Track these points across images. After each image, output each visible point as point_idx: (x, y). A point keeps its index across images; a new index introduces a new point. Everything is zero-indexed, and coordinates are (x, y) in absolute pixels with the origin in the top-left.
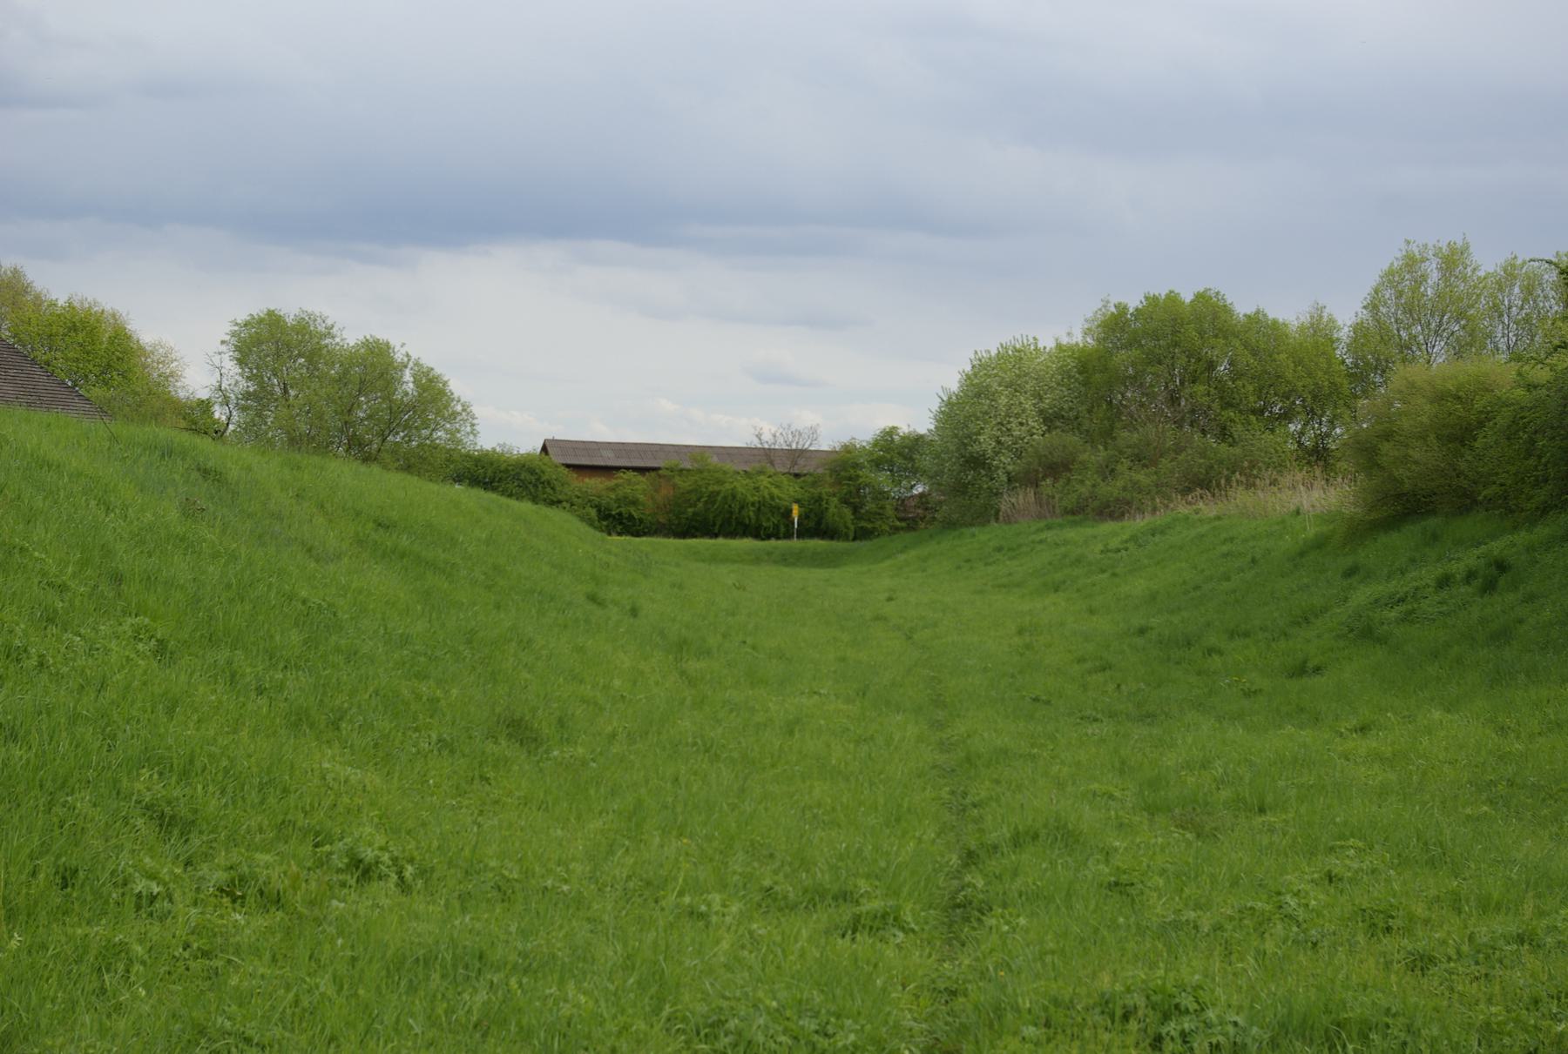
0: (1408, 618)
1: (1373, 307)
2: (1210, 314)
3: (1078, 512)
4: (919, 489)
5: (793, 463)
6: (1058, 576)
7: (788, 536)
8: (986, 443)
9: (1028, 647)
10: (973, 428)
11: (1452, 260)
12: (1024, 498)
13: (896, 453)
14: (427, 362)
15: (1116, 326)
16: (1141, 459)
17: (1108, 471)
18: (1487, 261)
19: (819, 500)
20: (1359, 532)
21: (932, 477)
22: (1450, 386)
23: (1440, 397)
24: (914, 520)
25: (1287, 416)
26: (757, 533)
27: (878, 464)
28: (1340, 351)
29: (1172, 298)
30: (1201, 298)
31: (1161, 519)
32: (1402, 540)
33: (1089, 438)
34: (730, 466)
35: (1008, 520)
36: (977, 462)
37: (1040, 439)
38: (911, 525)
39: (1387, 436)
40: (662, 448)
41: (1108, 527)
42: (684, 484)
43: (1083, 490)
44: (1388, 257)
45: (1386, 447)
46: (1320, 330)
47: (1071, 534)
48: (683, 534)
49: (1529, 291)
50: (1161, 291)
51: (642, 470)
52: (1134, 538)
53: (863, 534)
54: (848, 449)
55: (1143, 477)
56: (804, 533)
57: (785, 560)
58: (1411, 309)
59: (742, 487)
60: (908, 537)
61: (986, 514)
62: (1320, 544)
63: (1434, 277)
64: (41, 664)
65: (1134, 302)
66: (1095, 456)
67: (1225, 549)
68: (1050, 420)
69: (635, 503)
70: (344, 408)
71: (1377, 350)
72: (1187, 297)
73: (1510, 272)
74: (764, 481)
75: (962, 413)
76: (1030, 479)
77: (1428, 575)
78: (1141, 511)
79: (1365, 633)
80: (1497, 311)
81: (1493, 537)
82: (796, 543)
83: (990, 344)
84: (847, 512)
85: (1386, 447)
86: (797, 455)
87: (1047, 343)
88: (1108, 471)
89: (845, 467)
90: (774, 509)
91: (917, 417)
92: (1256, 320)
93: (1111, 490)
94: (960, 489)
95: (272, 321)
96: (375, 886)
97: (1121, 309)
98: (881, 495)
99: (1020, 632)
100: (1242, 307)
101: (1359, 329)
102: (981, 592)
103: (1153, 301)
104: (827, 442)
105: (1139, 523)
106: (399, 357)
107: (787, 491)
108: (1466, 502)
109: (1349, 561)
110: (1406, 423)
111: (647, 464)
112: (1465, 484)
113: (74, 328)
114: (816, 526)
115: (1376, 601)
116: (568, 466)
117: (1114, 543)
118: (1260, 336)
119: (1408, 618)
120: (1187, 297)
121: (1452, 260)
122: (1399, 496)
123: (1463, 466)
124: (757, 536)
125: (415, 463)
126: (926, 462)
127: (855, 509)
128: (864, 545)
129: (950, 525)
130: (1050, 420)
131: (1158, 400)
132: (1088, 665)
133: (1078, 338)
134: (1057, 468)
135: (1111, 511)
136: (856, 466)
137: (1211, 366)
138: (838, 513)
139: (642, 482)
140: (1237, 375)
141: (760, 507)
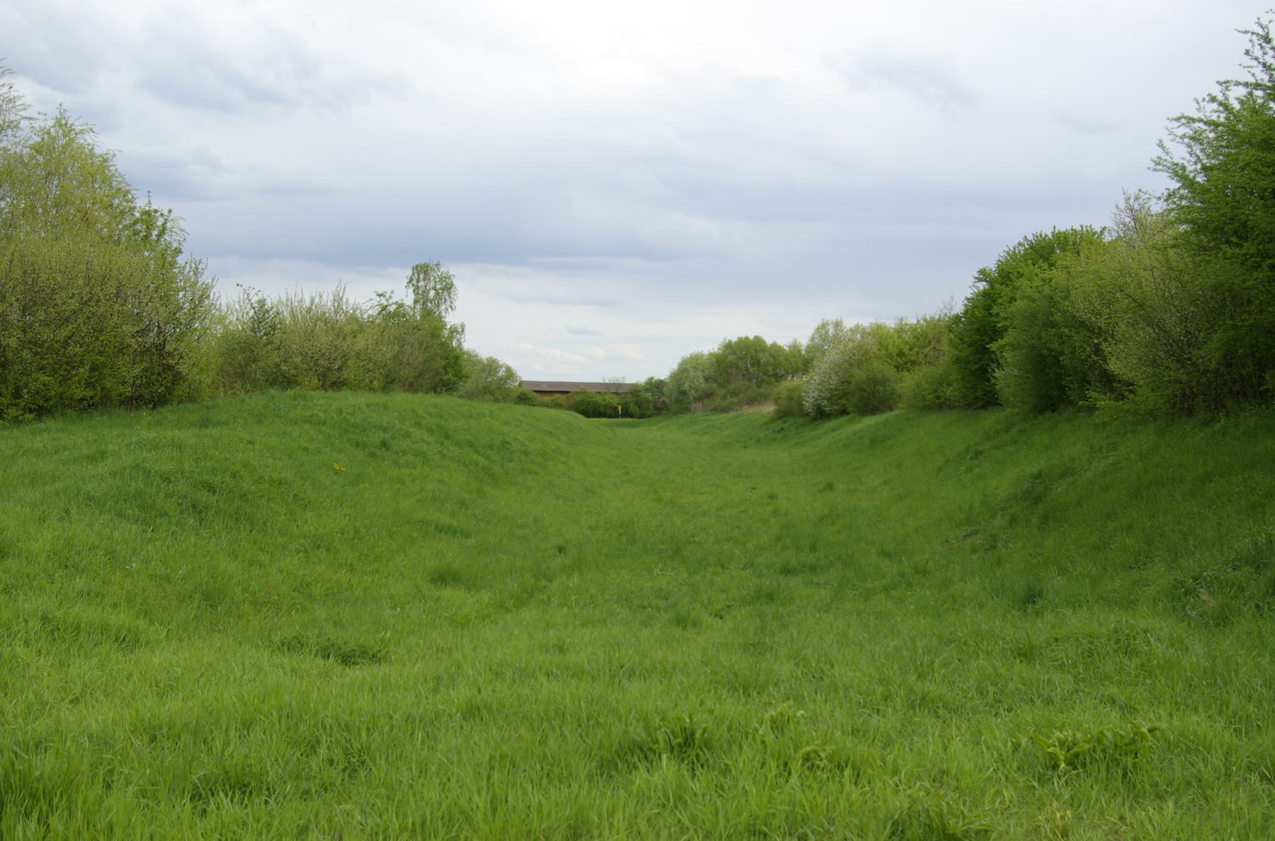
1: (812, 339)
2: (758, 342)
5: (616, 389)
7: (617, 416)
8: (686, 387)
11: (837, 325)
12: (699, 405)
13: (655, 386)
15: (729, 346)
16: (734, 394)
17: (724, 397)
20: (773, 420)
26: (610, 416)
27: (647, 390)
29: (747, 338)
33: (720, 385)
36: (684, 393)
41: (723, 415)
44: (817, 323)
46: (795, 347)
47: (712, 417)
50: (743, 336)
53: (642, 416)
55: (734, 400)
57: (619, 425)
59: (599, 399)
61: (687, 410)
64: (118, 295)
65: (734, 339)
66: (721, 392)
68: (707, 379)
71: (816, 349)
72: (752, 337)
74: (607, 397)
76: (699, 399)
86: (619, 385)
87: (706, 352)
88: (724, 397)
89: (634, 391)
92: (774, 345)
93: (725, 404)
94: (677, 401)
96: (1051, 708)
100: (769, 342)
103: (740, 339)
105: (732, 414)
107: (615, 400)
114: (626, 414)
120: (752, 337)
121: (837, 325)
128: (646, 420)
129: (676, 414)
131: (742, 373)
133: (716, 350)
134: (709, 395)
135: (725, 410)
138: (633, 408)
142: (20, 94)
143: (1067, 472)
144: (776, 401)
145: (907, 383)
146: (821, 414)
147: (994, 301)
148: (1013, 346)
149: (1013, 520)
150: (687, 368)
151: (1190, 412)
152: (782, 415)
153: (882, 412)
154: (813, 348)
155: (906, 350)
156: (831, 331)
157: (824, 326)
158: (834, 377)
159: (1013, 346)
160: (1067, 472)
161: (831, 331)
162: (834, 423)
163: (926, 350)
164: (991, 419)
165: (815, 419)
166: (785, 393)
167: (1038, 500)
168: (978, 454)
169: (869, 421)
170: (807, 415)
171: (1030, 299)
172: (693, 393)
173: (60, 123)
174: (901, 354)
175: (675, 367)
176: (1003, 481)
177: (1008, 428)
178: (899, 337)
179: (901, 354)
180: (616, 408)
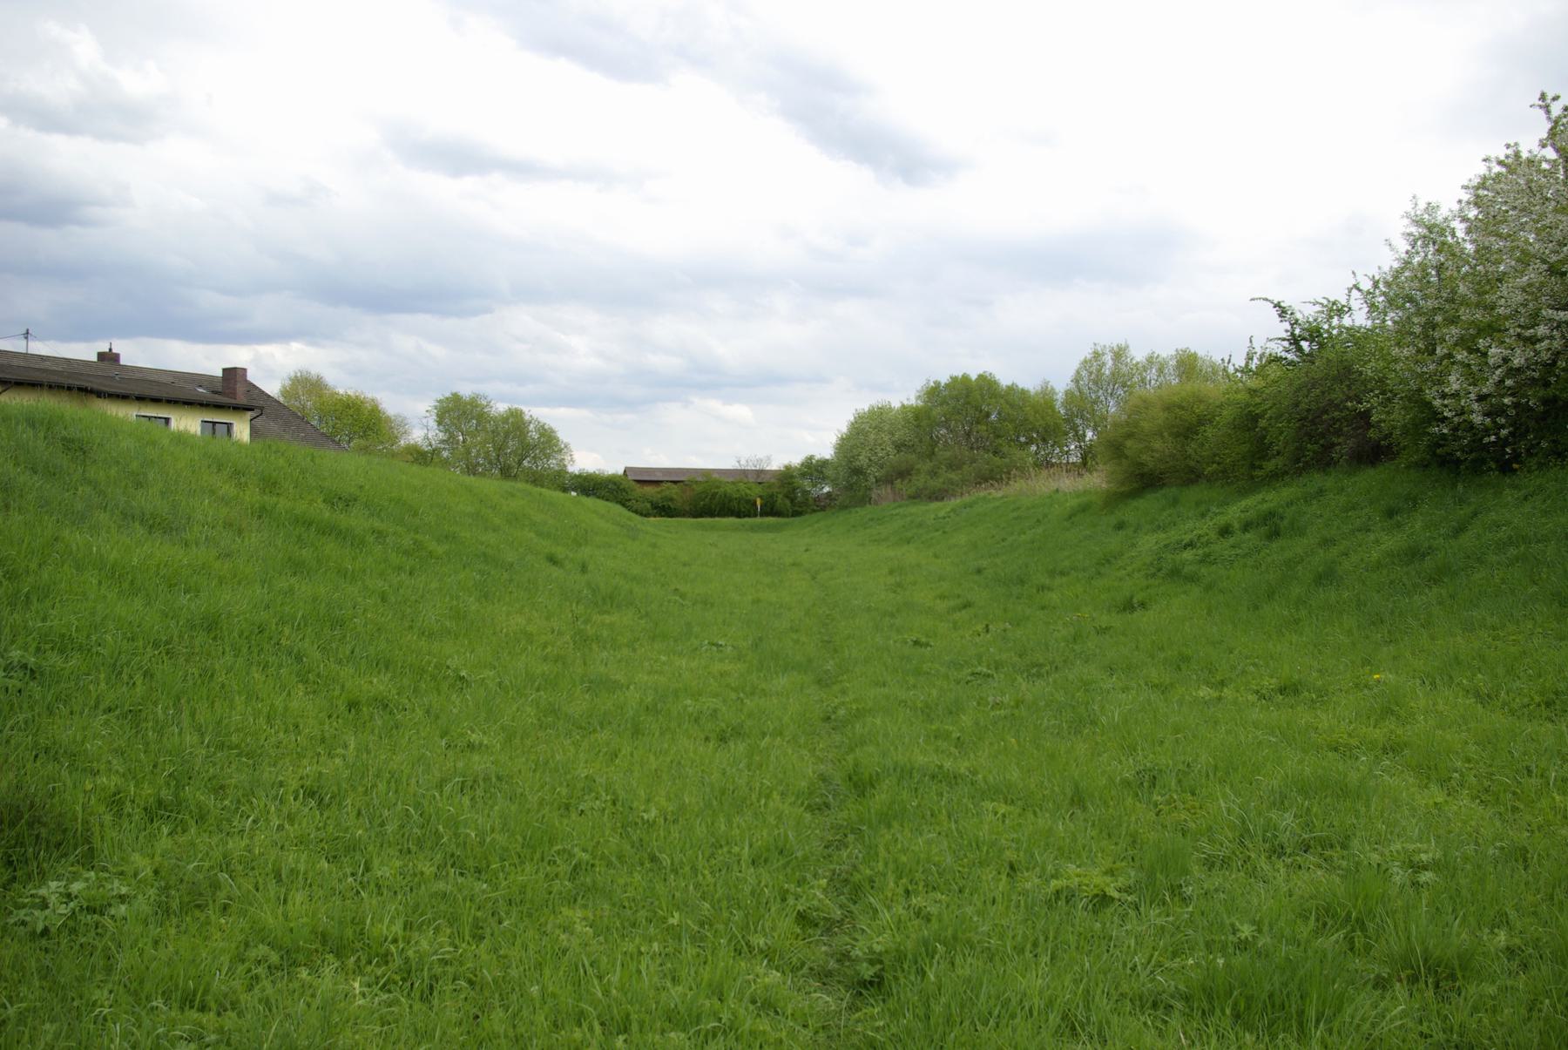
0: (1205, 560)
1: (1076, 381)
2: (986, 385)
3: (915, 497)
4: (827, 489)
6: (909, 534)
8: (863, 460)
9: (899, 585)
10: (855, 452)
12: (885, 491)
13: (814, 469)
14: (543, 420)
15: (934, 393)
16: (953, 466)
17: (933, 474)
18: (1138, 354)
19: (772, 496)
20: (1115, 500)
21: (834, 482)
22: (1175, 399)
23: (1168, 408)
24: (822, 505)
25: (1030, 441)
26: (739, 515)
27: (803, 475)
28: (1058, 405)
29: (966, 378)
30: (981, 377)
31: (967, 498)
32: (1149, 503)
34: (724, 479)
35: (876, 503)
36: (858, 471)
37: (894, 458)
38: (823, 509)
39: (1130, 436)
40: (688, 470)
41: (935, 505)
42: (699, 489)
43: (920, 485)
44: (1086, 352)
45: (1129, 443)
46: (1047, 394)
47: (913, 509)
48: (695, 516)
49: (1160, 371)
51: (675, 482)
52: (953, 510)
53: (796, 514)
54: (788, 468)
55: (953, 476)
56: (764, 514)
57: (753, 529)
58: (1097, 381)
59: (729, 489)
60: (820, 515)
61: (864, 500)
62: (1084, 509)
63: (1110, 363)
65: (944, 379)
66: (927, 466)
67: (1015, 514)
69: (671, 500)
70: (497, 447)
71: (1081, 405)
72: (974, 377)
73: (1151, 360)
74: (742, 486)
75: (851, 443)
76: (888, 480)
77: (1207, 527)
78: (954, 496)
81: (1225, 503)
82: (758, 520)
83: (864, 406)
84: (788, 502)
85: (1129, 443)
86: (760, 472)
87: (896, 405)
88: (933, 474)
89: (787, 477)
90: (748, 502)
91: (825, 449)
92: (1012, 389)
93: (936, 483)
94: (850, 487)
95: (456, 398)
97: (937, 384)
98: (806, 493)
99: (891, 572)
101: (1068, 393)
102: (863, 545)
103: (954, 379)
104: (776, 464)
105: (955, 502)
106: (527, 418)
108: (1192, 477)
109: (1113, 520)
110: (1145, 425)
111: (678, 479)
112: (1192, 464)
113: (348, 407)
114: (770, 510)
115: (1166, 546)
116: (638, 481)
117: (942, 514)
118: (1014, 399)
119: (1205, 560)
120: (974, 377)
121: (1119, 354)
122: (1142, 475)
123: (1190, 451)
124: (739, 516)
125: (536, 479)
126: (829, 472)
127: (792, 501)
128: (797, 519)
129: (844, 507)
130: (899, 446)
131: (959, 439)
132: (952, 603)
134: (904, 473)
135: (937, 496)
136: (792, 477)
137: (988, 415)
139: (675, 489)
140: (1001, 419)
141: (739, 500)
142: (1407, 221)
150: (866, 432)
156: (1108, 359)
172: (874, 472)
173: (1418, 222)
175: (845, 430)
180: (755, 503)
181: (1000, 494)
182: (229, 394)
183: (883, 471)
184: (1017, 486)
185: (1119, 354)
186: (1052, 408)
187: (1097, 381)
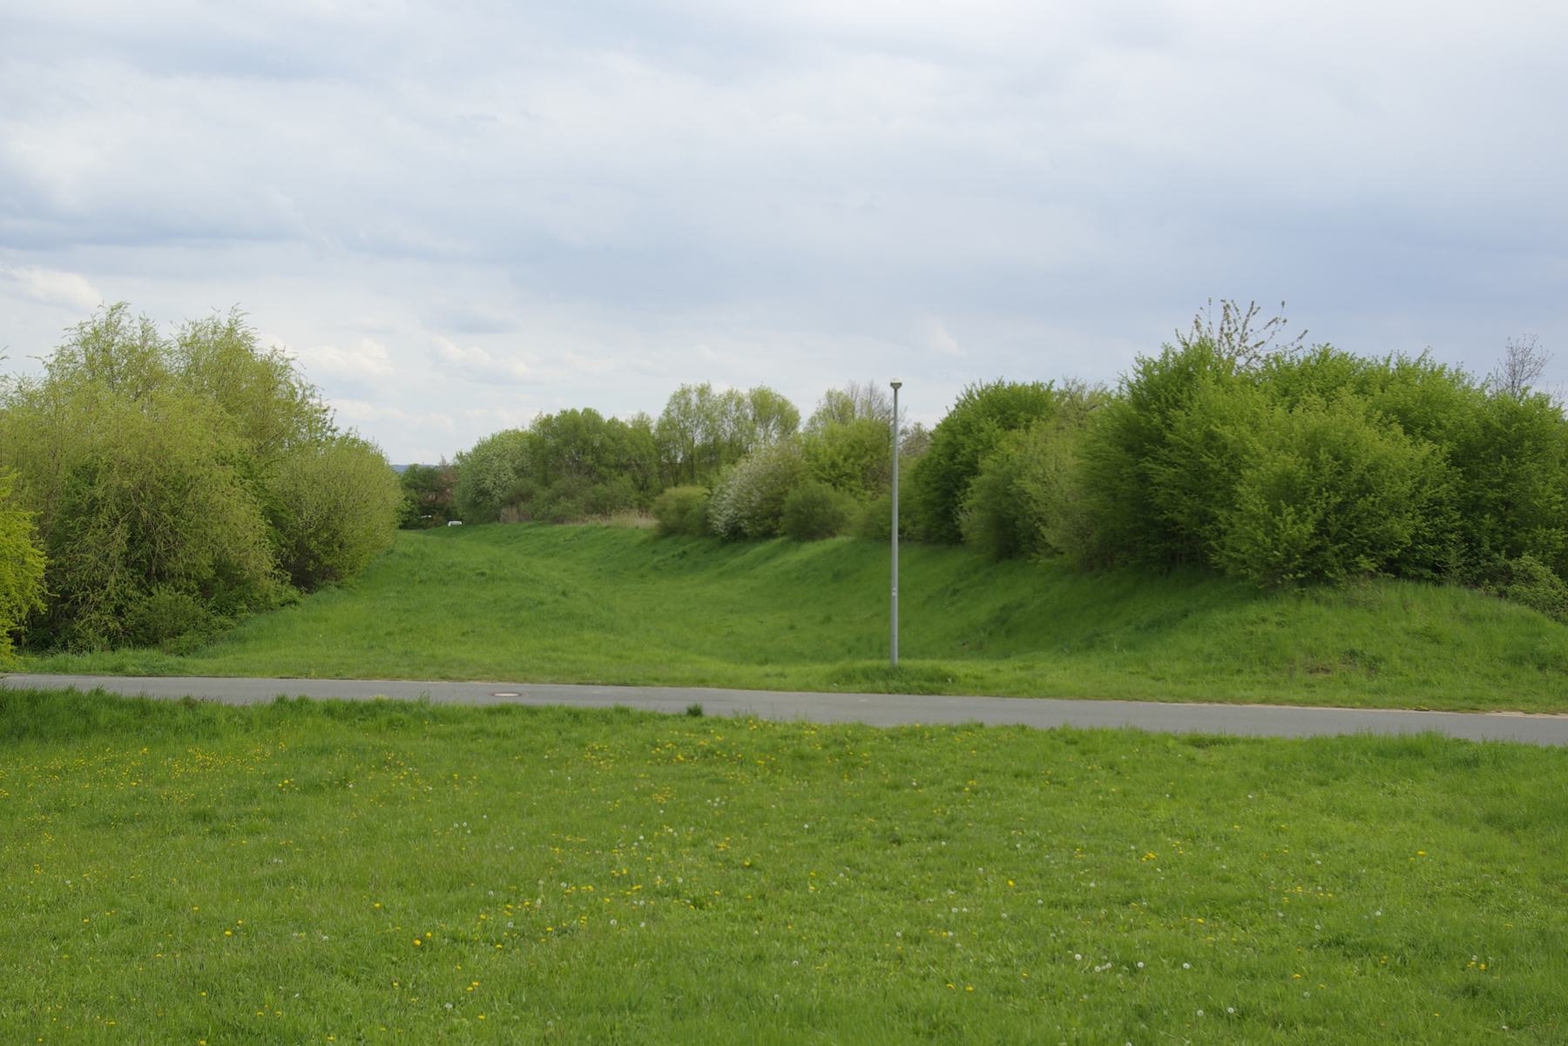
1: (668, 412)
2: (591, 417)
8: (488, 484)
20: (657, 539)
29: (574, 412)
30: (586, 410)
32: (668, 541)
35: (505, 522)
36: (484, 493)
37: (515, 481)
41: (558, 527)
46: (642, 425)
58: (686, 414)
62: (645, 542)
65: (555, 414)
68: (520, 472)
73: (731, 396)
76: (511, 502)
79: (656, 568)
80: (723, 413)
92: (613, 422)
118: (614, 430)
121: (703, 392)
130: (520, 472)
134: (526, 496)
143: (1020, 605)
144: (658, 514)
145: (853, 506)
146: (736, 536)
147: (957, 451)
148: (979, 507)
149: (991, 634)
150: (486, 454)
151: (1092, 568)
152: (668, 532)
153: (823, 537)
154: (668, 424)
155: (839, 460)
156: (694, 399)
157: (684, 393)
158: (755, 492)
159: (979, 507)
160: (1020, 605)
161: (694, 399)
162: (762, 548)
163: (863, 462)
164: (957, 559)
165: (725, 542)
166: (672, 505)
167: (1004, 622)
168: (955, 592)
169: (811, 550)
170: (714, 534)
171: (993, 472)
174: (834, 465)
176: (983, 610)
177: (976, 571)
178: (831, 445)
179: (834, 465)
181: (604, 524)
182: (1197, 700)
183: (507, 493)
184: (615, 520)
185: (703, 392)
186: (647, 429)
187: (686, 414)
